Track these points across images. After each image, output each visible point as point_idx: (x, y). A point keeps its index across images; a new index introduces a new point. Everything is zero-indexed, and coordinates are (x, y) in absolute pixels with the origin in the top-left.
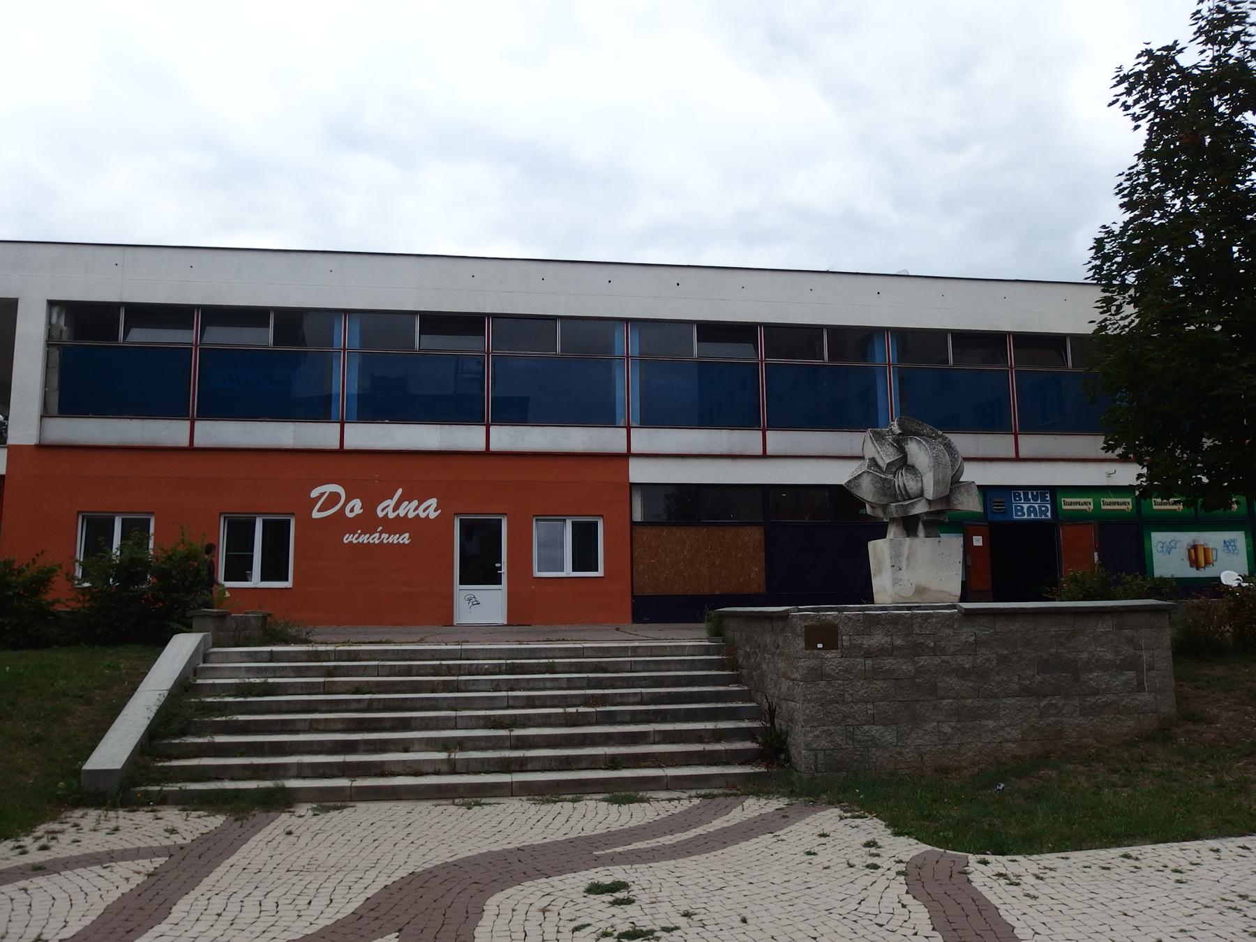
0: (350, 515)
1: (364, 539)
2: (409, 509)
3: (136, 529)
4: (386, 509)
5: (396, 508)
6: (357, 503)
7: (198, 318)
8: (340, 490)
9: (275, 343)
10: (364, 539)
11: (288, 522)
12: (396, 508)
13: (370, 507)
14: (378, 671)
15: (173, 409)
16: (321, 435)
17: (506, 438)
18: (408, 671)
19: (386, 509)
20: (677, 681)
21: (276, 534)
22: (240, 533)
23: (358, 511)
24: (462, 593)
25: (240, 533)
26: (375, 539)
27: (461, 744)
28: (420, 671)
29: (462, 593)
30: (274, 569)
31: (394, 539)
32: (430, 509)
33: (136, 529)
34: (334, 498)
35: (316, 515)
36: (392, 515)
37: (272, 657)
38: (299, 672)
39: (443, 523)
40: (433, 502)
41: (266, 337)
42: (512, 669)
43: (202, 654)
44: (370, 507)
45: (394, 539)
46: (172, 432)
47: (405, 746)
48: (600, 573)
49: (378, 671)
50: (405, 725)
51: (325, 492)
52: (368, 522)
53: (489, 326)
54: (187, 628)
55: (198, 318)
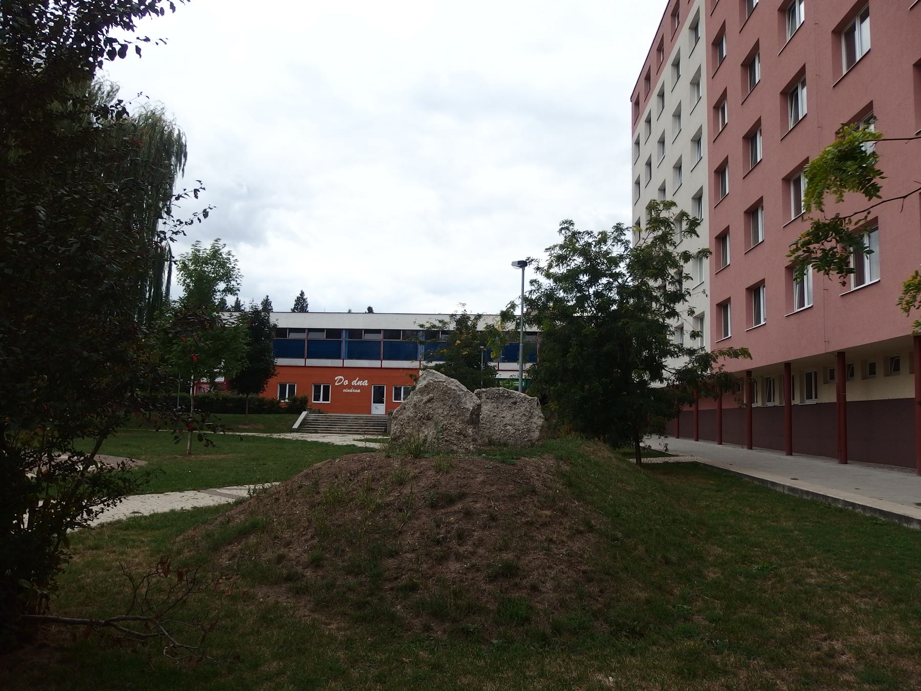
0: (345, 384)
1: (349, 391)
2: (360, 383)
3: (292, 388)
4: (354, 383)
5: (357, 382)
6: (347, 381)
7: (306, 331)
8: (343, 378)
9: (326, 338)
10: (349, 391)
11: (329, 386)
12: (357, 382)
13: (350, 383)
14: (334, 418)
15: (300, 355)
16: (337, 363)
17: (387, 364)
18: (339, 418)
19: (354, 383)
20: (381, 422)
21: (326, 389)
22: (317, 388)
23: (347, 383)
24: (374, 406)
25: (317, 388)
26: (351, 391)
27: (343, 428)
28: (341, 419)
29: (374, 406)
30: (326, 398)
31: (356, 391)
32: (366, 383)
33: (292, 388)
34: (341, 380)
35: (336, 384)
36: (356, 385)
37: (318, 416)
38: (322, 418)
39: (369, 387)
40: (366, 381)
41: (323, 336)
42: (356, 419)
43: (307, 415)
44: (350, 383)
45: (356, 391)
46: (300, 362)
47: (335, 428)
48: (329, 402)
49: (334, 418)
50: (336, 425)
51: (701, 189)
52: (349, 386)
53: (382, 332)
54: (305, 411)
55: (306, 331)
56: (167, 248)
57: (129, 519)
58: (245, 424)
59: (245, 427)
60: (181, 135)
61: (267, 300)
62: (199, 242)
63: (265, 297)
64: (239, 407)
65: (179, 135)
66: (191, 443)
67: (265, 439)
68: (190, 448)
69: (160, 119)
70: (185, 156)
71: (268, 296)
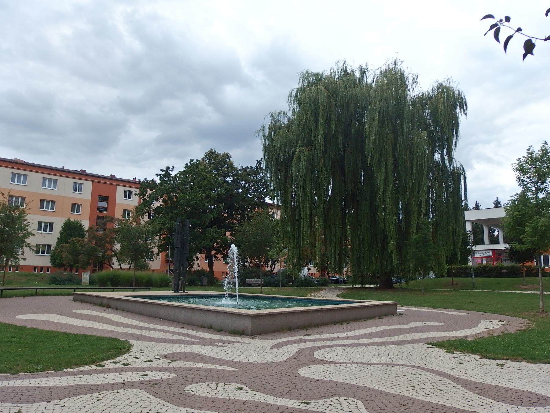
56: (462, 168)
57: (320, 291)
58: (524, 285)
59: (525, 287)
60: (461, 93)
61: (497, 200)
62: (532, 146)
63: (495, 199)
64: (513, 273)
65: (459, 93)
66: (543, 302)
67: (507, 293)
68: (543, 307)
69: (449, 88)
70: (466, 105)
71: (497, 198)
